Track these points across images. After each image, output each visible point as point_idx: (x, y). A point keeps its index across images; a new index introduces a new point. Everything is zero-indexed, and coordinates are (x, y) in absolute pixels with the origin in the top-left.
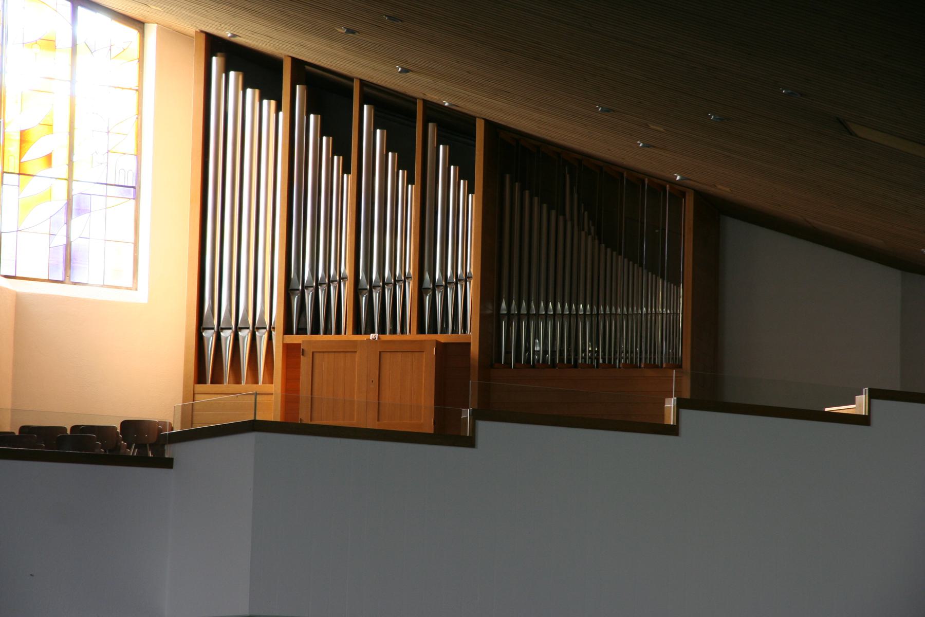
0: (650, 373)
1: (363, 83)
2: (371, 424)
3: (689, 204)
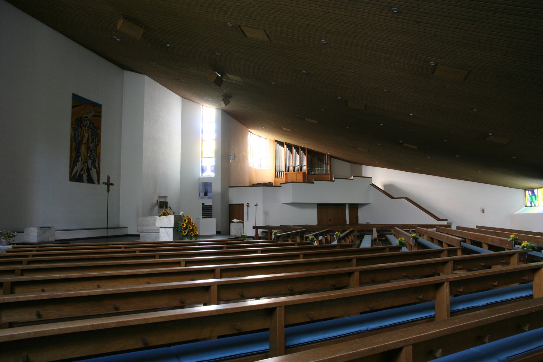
0: (325, 175)
1: (293, 145)
2: (296, 181)
3: (329, 156)
